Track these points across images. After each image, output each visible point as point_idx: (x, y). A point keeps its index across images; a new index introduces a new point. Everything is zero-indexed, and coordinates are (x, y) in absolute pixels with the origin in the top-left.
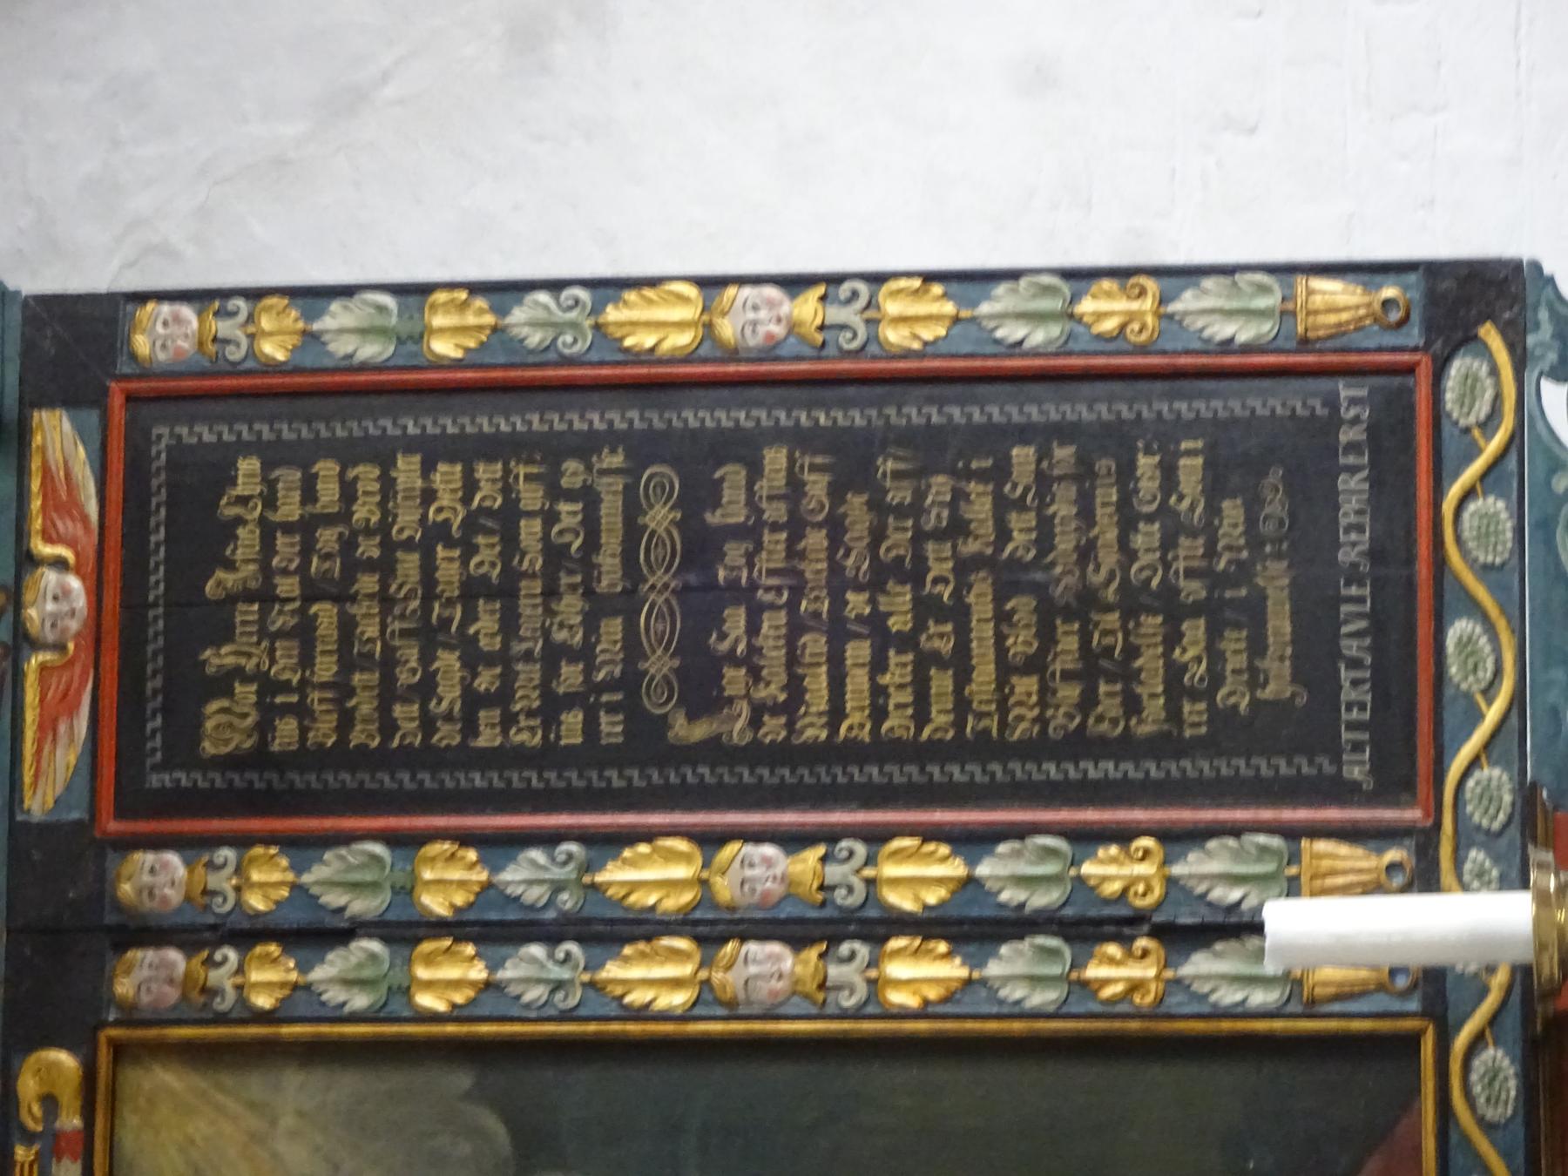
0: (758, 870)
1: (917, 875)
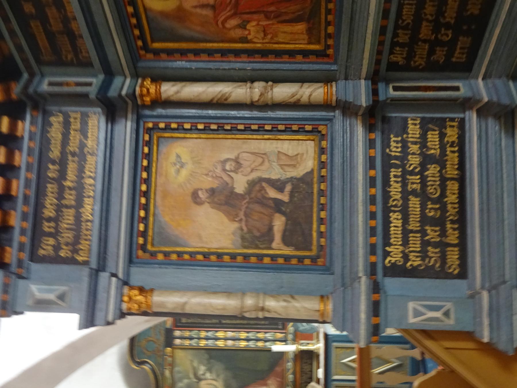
0: (230, 334)
1: (243, 335)
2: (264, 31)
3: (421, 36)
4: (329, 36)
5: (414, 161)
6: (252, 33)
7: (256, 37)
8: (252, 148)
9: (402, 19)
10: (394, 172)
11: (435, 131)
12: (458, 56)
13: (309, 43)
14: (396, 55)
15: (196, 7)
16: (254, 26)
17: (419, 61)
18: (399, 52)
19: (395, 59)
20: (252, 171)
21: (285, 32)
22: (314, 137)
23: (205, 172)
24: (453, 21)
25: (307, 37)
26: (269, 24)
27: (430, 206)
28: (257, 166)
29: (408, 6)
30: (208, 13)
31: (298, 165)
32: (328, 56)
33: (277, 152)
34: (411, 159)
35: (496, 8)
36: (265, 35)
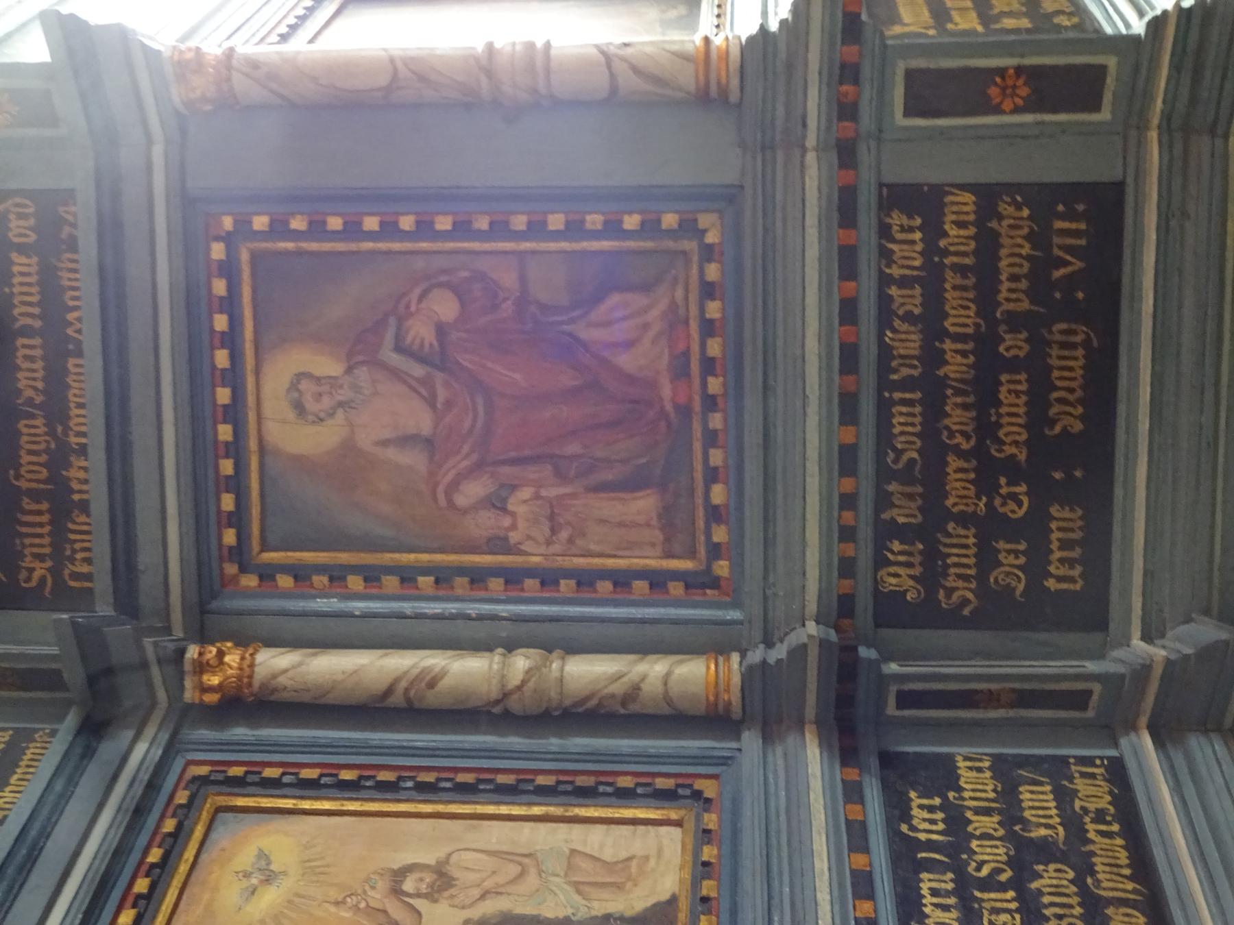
2: (552, 517)
3: (949, 502)
4: (715, 514)
5: (989, 855)
6: (521, 524)
7: (529, 537)
8: (494, 840)
9: (894, 449)
10: (930, 880)
11: (1041, 784)
12: (1062, 575)
13: (669, 555)
14: (892, 570)
15: (385, 443)
16: (525, 502)
17: (960, 590)
18: (901, 558)
19: (893, 581)
20: (483, 897)
21: (603, 521)
22: (683, 812)
23: (334, 894)
24: (1022, 457)
25: (661, 537)
26: (566, 495)
27: (1004, 491)
28: (498, 885)
29: (904, 409)
30: (414, 459)
31: (629, 885)
32: (715, 583)
33: (568, 852)
34: (977, 849)
35: (1122, 409)
36: (553, 531)
